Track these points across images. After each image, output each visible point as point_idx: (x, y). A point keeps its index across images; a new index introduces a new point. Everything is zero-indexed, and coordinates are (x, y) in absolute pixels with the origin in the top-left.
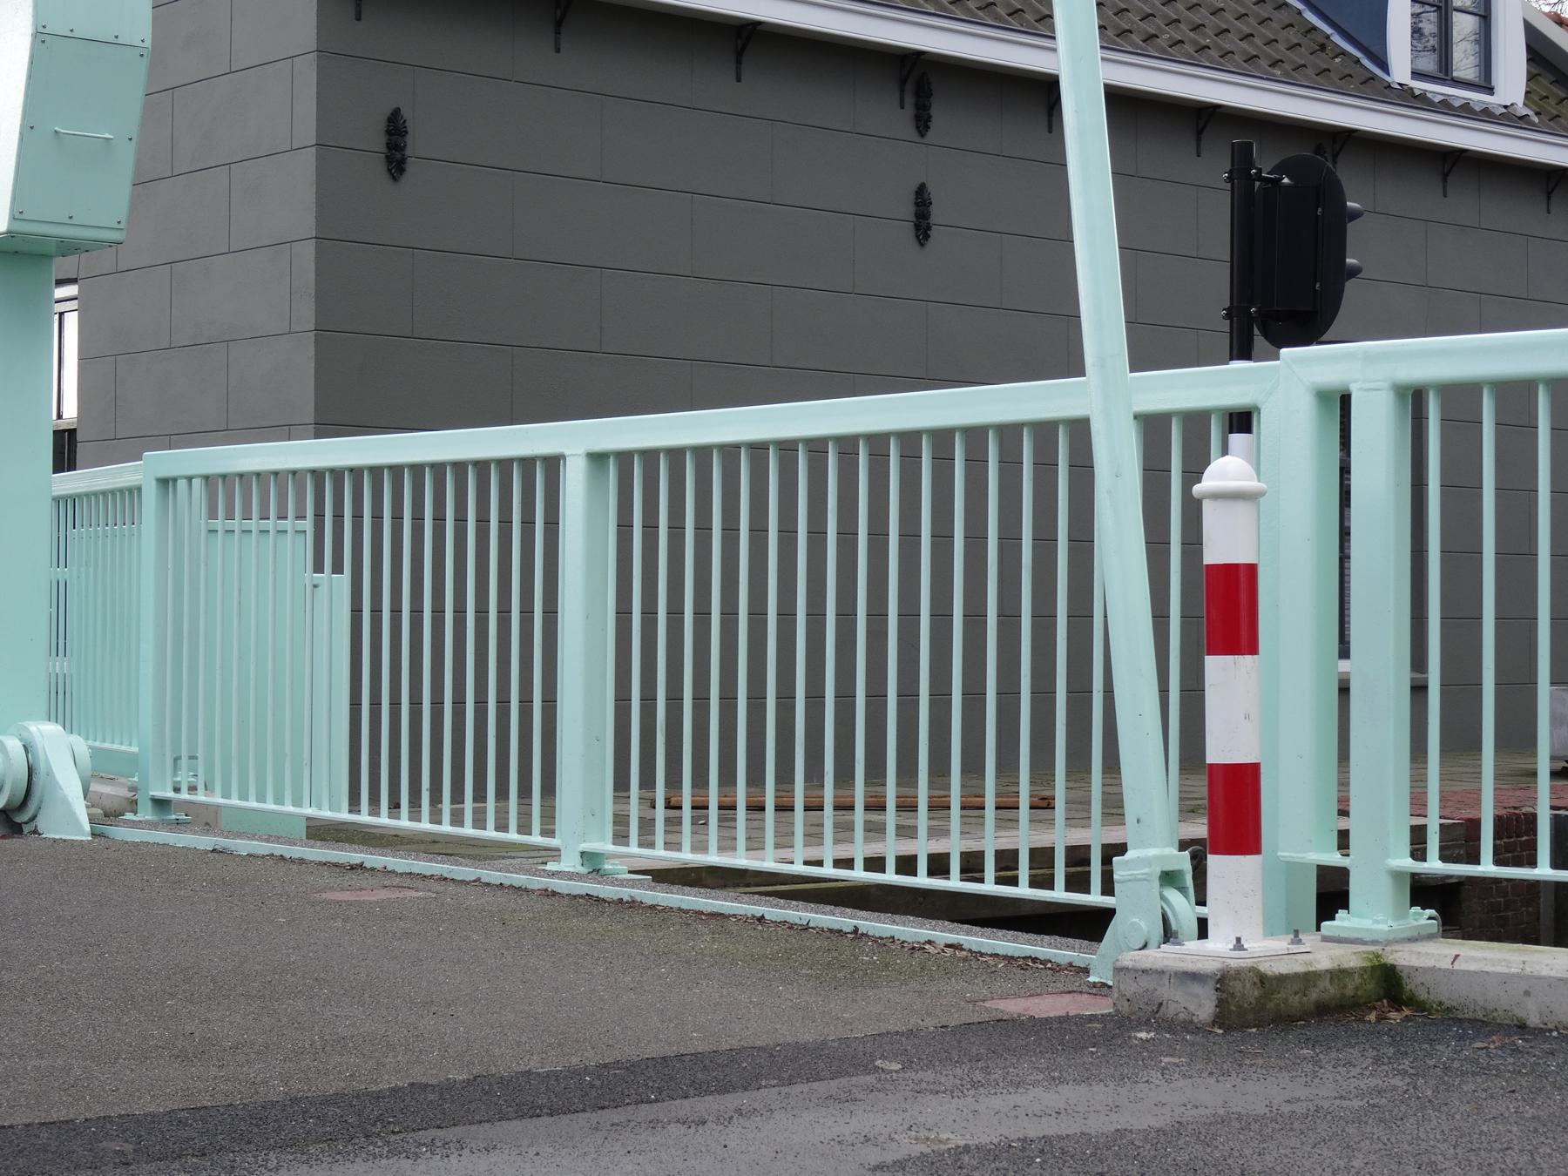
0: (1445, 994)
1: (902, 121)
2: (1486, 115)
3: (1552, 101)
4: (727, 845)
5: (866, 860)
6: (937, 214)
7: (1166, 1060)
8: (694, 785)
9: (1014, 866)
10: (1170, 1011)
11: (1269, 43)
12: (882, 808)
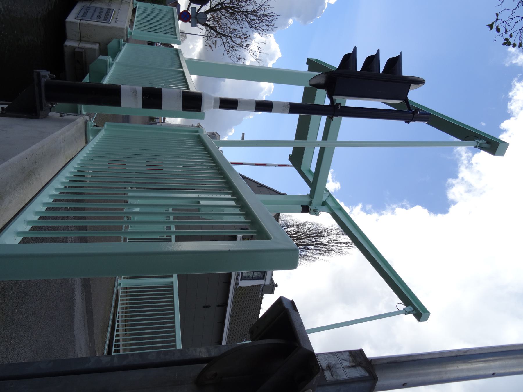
2: (237, 280)
4: (122, 304)
5: (119, 325)
8: (130, 295)
9: (117, 342)
11: (233, 333)
12: (126, 309)
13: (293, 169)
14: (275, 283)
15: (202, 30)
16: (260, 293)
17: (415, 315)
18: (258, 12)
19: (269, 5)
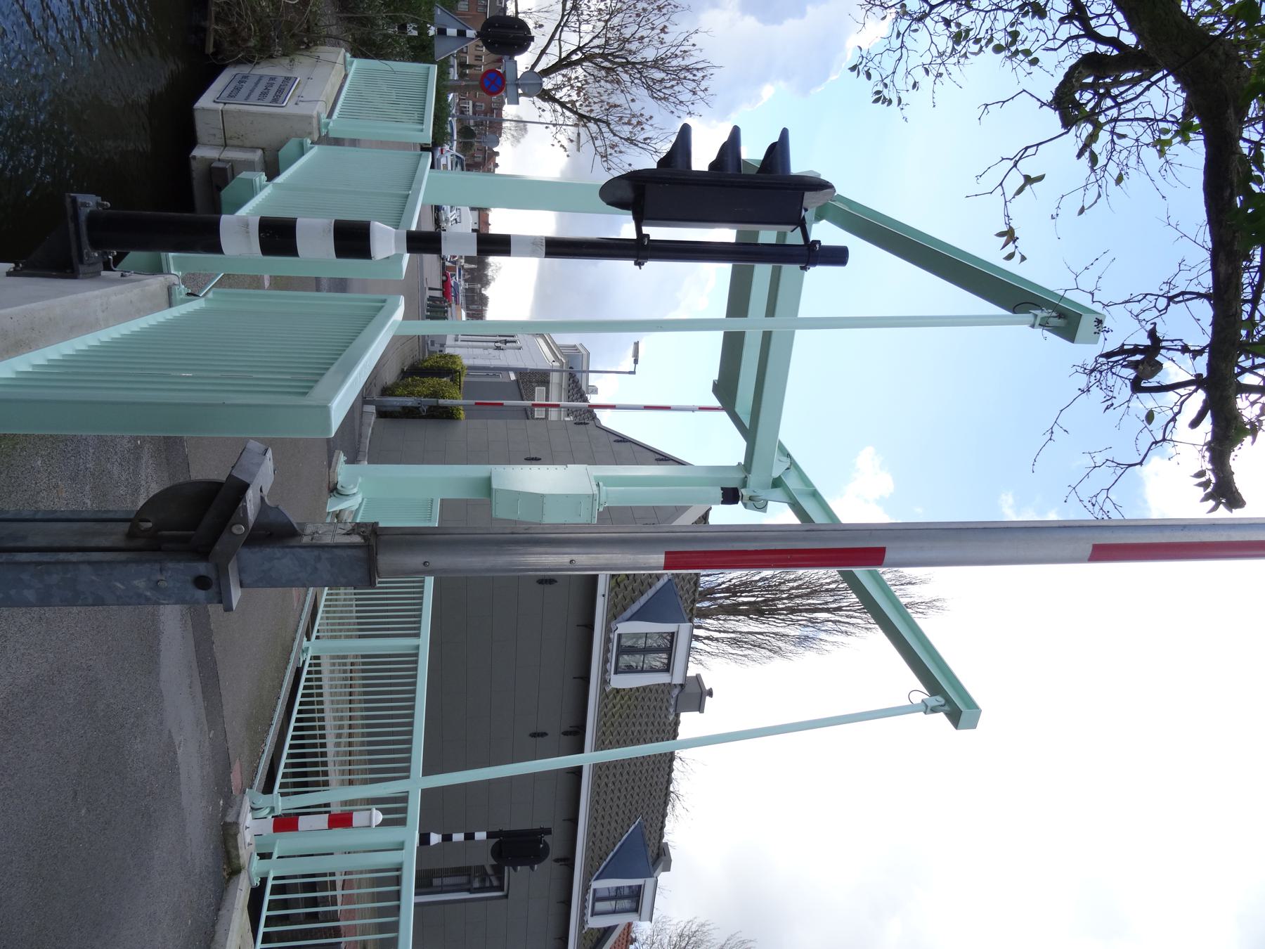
0: (231, 887)
1: (566, 727)
3: (591, 937)
6: (539, 739)
7: (211, 808)
10: (230, 810)
13: (724, 415)
14: (707, 688)
15: (544, 110)
16: (671, 710)
17: (949, 715)
18: (669, 62)
19: (694, 45)
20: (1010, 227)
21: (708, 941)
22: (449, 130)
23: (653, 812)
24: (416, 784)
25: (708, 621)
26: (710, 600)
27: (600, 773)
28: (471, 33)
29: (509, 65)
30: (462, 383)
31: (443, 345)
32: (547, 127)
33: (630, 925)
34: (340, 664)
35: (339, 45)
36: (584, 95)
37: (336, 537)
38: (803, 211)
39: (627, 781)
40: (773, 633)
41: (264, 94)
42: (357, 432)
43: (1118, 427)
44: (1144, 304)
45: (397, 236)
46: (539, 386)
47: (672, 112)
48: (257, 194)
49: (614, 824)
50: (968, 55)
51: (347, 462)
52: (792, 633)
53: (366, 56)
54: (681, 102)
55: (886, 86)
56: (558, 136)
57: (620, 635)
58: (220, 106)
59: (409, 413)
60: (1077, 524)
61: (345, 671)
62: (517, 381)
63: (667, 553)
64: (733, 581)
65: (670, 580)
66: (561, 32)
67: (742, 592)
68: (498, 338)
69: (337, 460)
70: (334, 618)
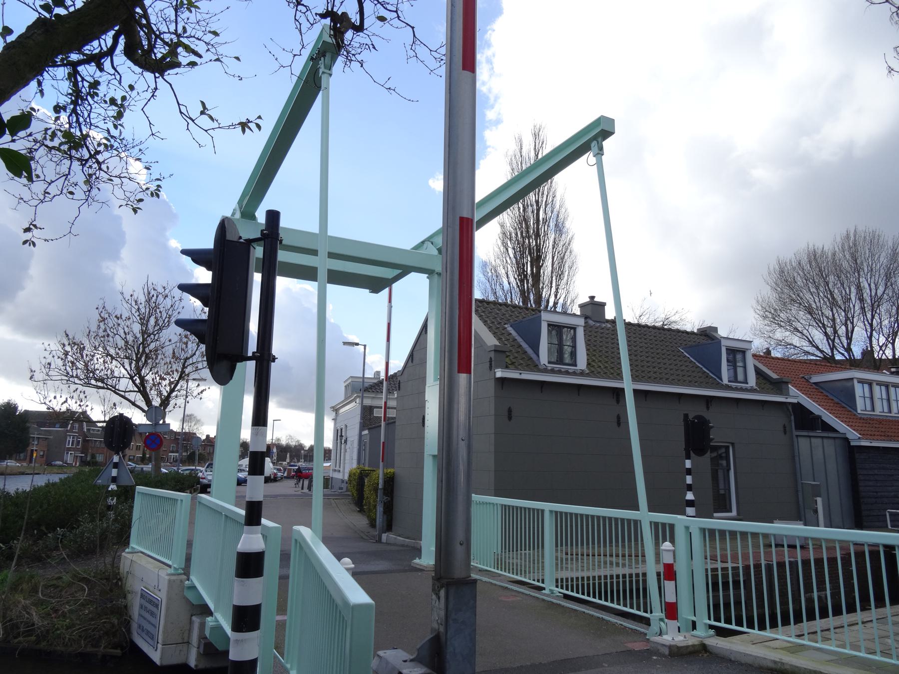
13: (395, 286)
14: (588, 300)
15: (176, 404)
16: (604, 325)
17: (605, 138)
20: (239, 124)
21: (769, 298)
22: (188, 472)
23: (675, 339)
24: (645, 516)
25: (544, 295)
26: (529, 294)
27: (646, 378)
28: (116, 459)
29: (141, 430)
30: (369, 469)
31: (343, 481)
32: (188, 402)
33: (754, 356)
34: (567, 563)
35: (120, 556)
36: (165, 374)
37: (441, 607)
38: (242, 240)
39: (653, 358)
40: (553, 249)
41: (152, 614)
42: (401, 548)
43: (388, 41)
44: (303, 20)
45: (249, 533)
46: (373, 414)
47: (179, 313)
48: (220, 625)
49: (683, 368)
50: (121, 138)
51: (420, 558)
52: (553, 236)
53: (129, 537)
54: (172, 306)
55: (147, 189)
56: (194, 394)
57: (549, 363)
58: (160, 646)
59: (389, 509)
60: (448, 80)
61: (572, 559)
62: (369, 429)
63: (459, 372)
64: (516, 276)
65: (511, 326)
66: (119, 391)
67: (524, 270)
68: (339, 441)
69: (418, 564)
70: (534, 568)
